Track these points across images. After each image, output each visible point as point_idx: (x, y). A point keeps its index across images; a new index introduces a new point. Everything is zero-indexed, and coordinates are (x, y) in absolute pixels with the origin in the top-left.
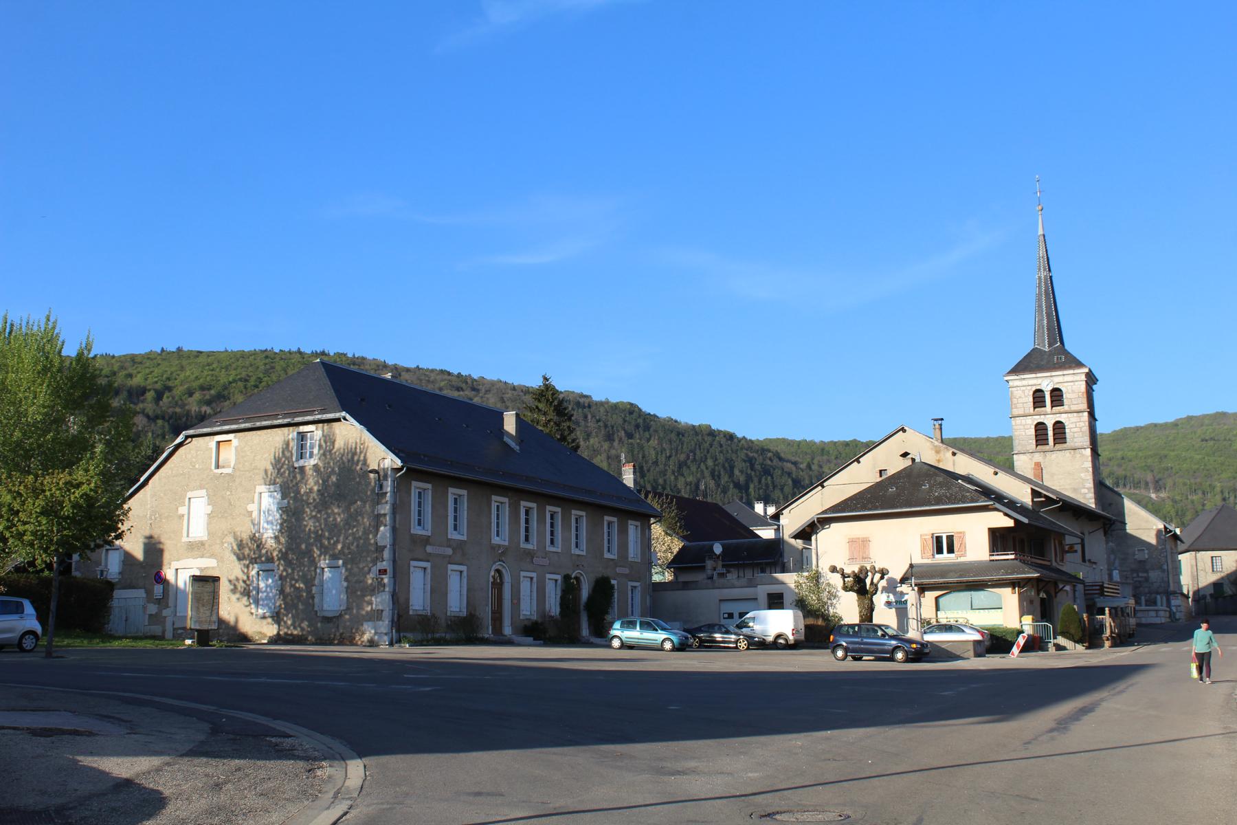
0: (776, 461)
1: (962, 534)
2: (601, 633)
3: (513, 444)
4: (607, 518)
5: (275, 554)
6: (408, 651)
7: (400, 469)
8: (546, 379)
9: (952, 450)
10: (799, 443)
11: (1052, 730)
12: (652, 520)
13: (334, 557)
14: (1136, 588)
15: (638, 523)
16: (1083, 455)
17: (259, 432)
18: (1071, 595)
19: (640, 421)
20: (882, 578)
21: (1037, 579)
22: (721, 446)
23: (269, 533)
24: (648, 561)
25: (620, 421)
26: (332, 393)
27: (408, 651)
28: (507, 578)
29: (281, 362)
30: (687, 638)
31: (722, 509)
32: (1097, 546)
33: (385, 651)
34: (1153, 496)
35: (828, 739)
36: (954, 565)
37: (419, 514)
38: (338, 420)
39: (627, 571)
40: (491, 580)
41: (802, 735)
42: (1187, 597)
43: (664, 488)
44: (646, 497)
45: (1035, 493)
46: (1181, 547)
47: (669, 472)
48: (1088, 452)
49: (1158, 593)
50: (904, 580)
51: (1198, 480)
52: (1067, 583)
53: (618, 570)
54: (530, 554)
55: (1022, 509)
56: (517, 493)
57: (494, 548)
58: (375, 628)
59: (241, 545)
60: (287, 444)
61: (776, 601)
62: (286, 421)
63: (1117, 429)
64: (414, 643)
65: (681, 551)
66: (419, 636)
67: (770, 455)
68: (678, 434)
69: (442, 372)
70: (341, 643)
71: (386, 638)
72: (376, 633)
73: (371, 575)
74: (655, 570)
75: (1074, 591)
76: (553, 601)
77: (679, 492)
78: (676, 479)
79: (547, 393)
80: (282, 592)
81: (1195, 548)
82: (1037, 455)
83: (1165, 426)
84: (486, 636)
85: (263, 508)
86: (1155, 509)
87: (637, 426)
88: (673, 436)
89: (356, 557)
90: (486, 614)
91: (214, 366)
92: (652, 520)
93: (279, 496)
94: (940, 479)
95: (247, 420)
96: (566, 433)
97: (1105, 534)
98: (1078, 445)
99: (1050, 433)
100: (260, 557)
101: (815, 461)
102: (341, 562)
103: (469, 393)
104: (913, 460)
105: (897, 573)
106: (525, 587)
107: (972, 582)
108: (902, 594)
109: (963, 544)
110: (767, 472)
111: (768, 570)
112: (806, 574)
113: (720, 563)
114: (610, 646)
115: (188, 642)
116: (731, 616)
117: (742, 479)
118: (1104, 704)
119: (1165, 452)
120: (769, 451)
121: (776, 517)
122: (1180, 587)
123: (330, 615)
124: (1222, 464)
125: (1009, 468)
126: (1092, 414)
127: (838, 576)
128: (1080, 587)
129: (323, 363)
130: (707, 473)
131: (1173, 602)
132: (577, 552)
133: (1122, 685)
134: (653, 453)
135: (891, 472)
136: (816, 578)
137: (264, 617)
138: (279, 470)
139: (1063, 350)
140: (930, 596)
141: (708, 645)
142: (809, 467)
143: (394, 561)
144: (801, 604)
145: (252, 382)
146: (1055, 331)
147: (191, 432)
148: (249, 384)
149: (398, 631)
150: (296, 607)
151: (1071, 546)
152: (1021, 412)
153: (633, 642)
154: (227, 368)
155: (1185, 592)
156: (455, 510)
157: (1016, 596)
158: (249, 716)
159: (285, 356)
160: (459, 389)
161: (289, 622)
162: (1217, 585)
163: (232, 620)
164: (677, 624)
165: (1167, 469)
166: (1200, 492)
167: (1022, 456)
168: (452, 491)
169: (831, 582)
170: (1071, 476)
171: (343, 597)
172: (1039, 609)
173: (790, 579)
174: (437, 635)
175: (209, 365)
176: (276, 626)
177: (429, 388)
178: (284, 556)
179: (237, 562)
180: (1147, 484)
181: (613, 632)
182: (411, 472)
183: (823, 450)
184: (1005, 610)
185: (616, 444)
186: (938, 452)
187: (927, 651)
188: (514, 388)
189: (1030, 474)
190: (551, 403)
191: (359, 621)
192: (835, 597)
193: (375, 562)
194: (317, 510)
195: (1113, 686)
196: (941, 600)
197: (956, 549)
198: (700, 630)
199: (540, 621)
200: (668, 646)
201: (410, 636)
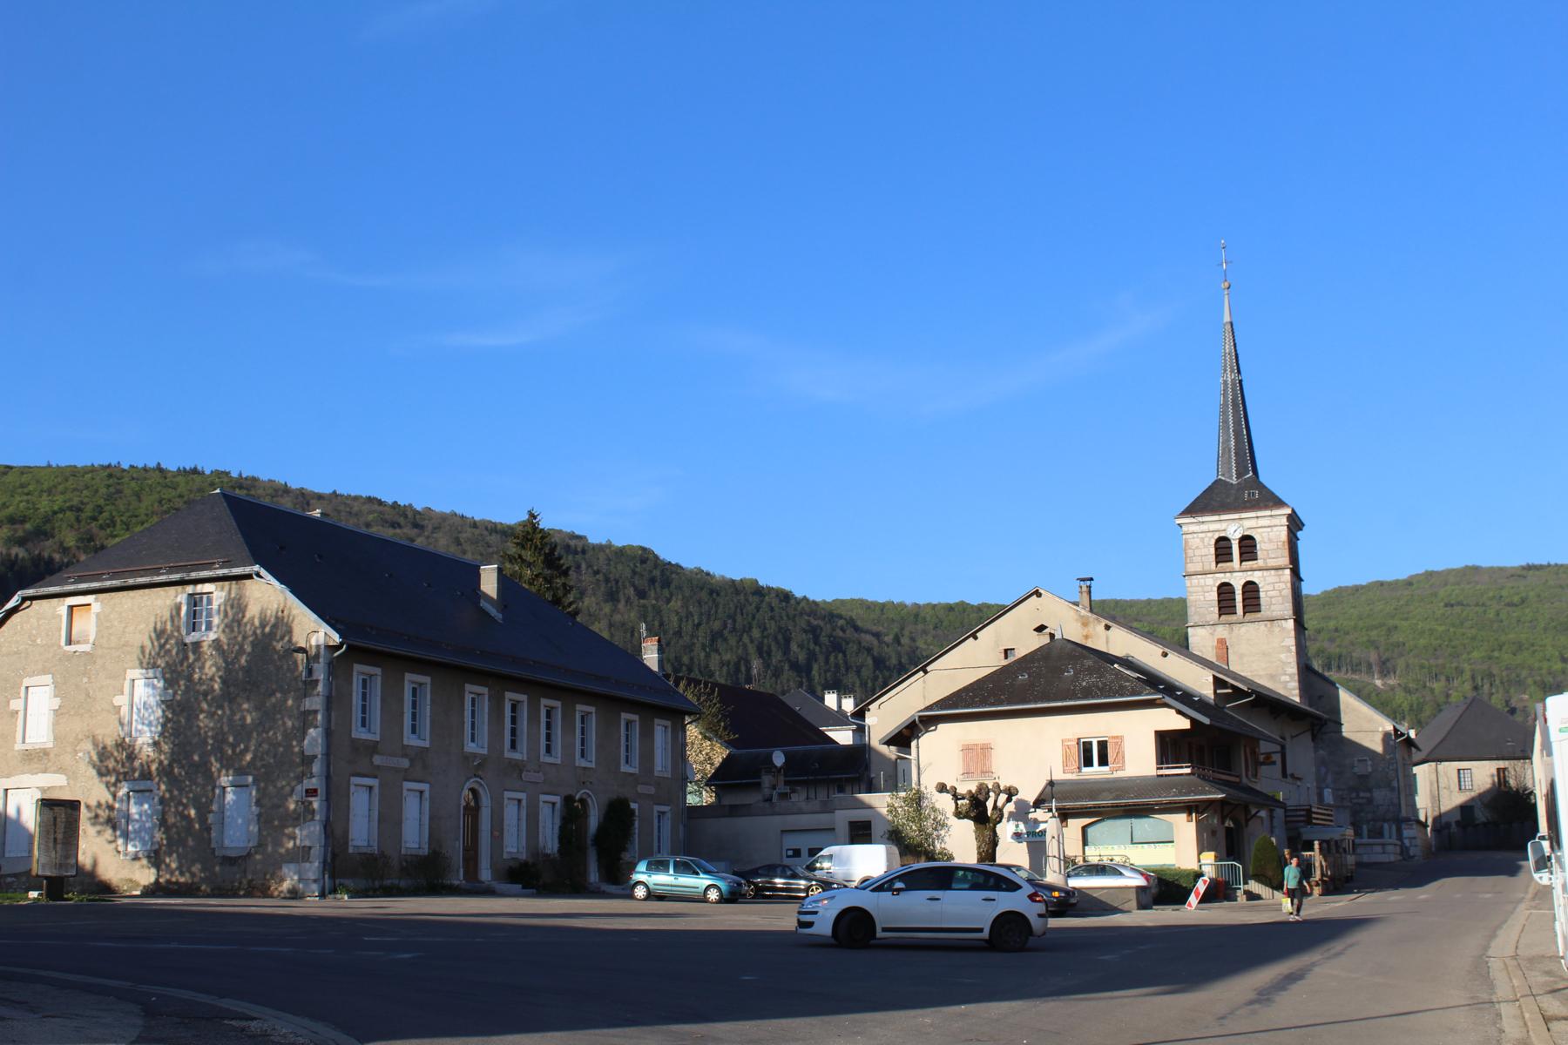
0: (850, 632)
1: (1119, 739)
2: (617, 879)
3: (493, 612)
4: (625, 716)
5: (154, 767)
6: (345, 905)
7: (338, 647)
8: (533, 516)
9: (1105, 622)
10: (884, 605)
11: (1251, 1002)
12: (687, 719)
13: (241, 772)
14: (1355, 813)
15: (668, 723)
16: (1283, 629)
17: (125, 593)
18: (1267, 823)
19: (657, 573)
20: (1009, 800)
21: (1221, 801)
22: (772, 609)
23: (144, 738)
24: (681, 775)
25: (628, 573)
26: (239, 538)
27: (345, 905)
28: (486, 801)
29: (133, 484)
30: (739, 885)
31: (778, 696)
32: (1303, 755)
33: (313, 905)
34: (1378, 683)
35: (963, 1015)
36: (1108, 781)
37: (364, 712)
38: (249, 577)
39: (652, 790)
40: (463, 803)
41: (929, 1010)
42: (1425, 825)
43: (690, 670)
44: (677, 685)
45: (1218, 683)
46: (1417, 756)
47: (698, 646)
48: (1290, 624)
49: (1385, 820)
50: (1038, 803)
51: (1440, 661)
52: (1261, 806)
53: (640, 789)
54: (518, 767)
55: (1199, 704)
56: (499, 680)
57: (467, 758)
58: (299, 873)
59: (103, 754)
60: (178, 608)
61: (861, 833)
62: (175, 577)
63: (1329, 588)
64: (355, 894)
65: (725, 760)
66: (362, 884)
67: (841, 622)
68: (711, 592)
69: (370, 500)
70: (249, 894)
71: (315, 887)
72: (300, 880)
73: (294, 798)
74: (690, 787)
75: (1272, 818)
76: (549, 832)
77: (712, 675)
78: (708, 656)
79: (530, 535)
80: (163, 822)
81: (1436, 757)
82: (1220, 628)
83: (1393, 586)
84: (456, 883)
85: (136, 699)
86: (1380, 703)
87: (652, 581)
88: (704, 595)
89: (268, 775)
90: (455, 850)
91: (31, 488)
92: (687, 719)
93: (161, 684)
94: (1089, 663)
95: (114, 576)
96: (560, 593)
97: (1314, 738)
98: (1276, 614)
99: (1239, 597)
100: (134, 770)
101: (906, 632)
102: (250, 779)
103: (409, 531)
104: (1052, 636)
105: (1029, 794)
106: (510, 812)
107: (1131, 805)
108: (1037, 822)
109: (1121, 756)
110: (837, 646)
111: (848, 789)
112: (903, 794)
113: (782, 778)
114: (631, 896)
115: (33, 894)
116: (797, 853)
117: (802, 657)
118: (1317, 969)
119: (1396, 622)
120: (840, 617)
121: (860, 714)
122: (1415, 810)
123: (233, 854)
124: (1474, 638)
125: (1181, 645)
126: (1295, 572)
127: (948, 797)
128: (1279, 812)
129: (224, 495)
130: (752, 649)
131: (1406, 833)
132: (584, 764)
133: (1338, 945)
134: (675, 619)
135: (1021, 652)
136: (918, 799)
137: (136, 858)
138: (162, 646)
139: (1256, 482)
140: (1075, 824)
141: (763, 895)
142: (897, 640)
143: (328, 777)
144: (895, 837)
145: (88, 511)
146: (1246, 456)
147: (30, 592)
148: (83, 516)
149: (332, 877)
150: (183, 843)
151: (1268, 755)
152: (1199, 568)
153: (660, 890)
154: (50, 492)
155: (1422, 818)
156: (414, 703)
157: (1193, 825)
158: (186, 994)
159: (140, 475)
160: (395, 525)
161: (174, 865)
162: (1465, 809)
163: (88, 867)
164: (722, 865)
165: (1398, 645)
166: (1443, 678)
167: (1200, 631)
168: (410, 679)
169: (937, 806)
170: (1267, 658)
171: (254, 828)
172: (1223, 843)
173: (880, 802)
174: (388, 882)
175: (22, 486)
176: (153, 871)
177: (350, 524)
178: (166, 772)
179: (96, 779)
180: (1370, 666)
181: (637, 877)
182: (357, 648)
183: (917, 616)
184: (1177, 845)
185: (621, 606)
186: (1085, 624)
187: (1073, 901)
188: (475, 525)
189: (1210, 655)
190: (544, 553)
191: (274, 866)
192: (943, 825)
193: (300, 779)
194: (218, 706)
195: (1326, 947)
196: (1090, 831)
197: (1110, 759)
198: (756, 873)
199: (530, 861)
200: (713, 895)
201: (349, 882)
